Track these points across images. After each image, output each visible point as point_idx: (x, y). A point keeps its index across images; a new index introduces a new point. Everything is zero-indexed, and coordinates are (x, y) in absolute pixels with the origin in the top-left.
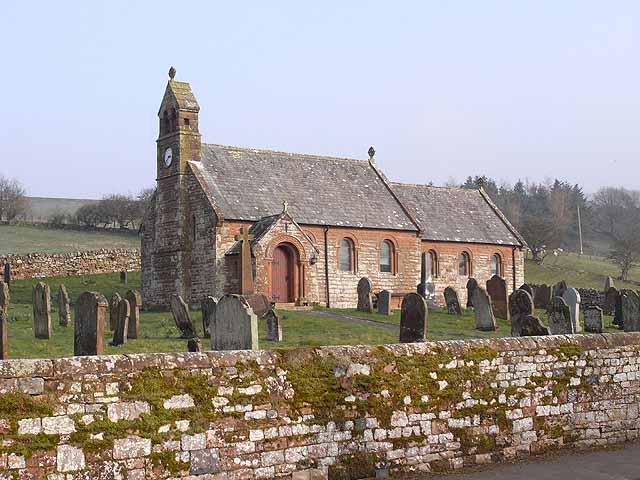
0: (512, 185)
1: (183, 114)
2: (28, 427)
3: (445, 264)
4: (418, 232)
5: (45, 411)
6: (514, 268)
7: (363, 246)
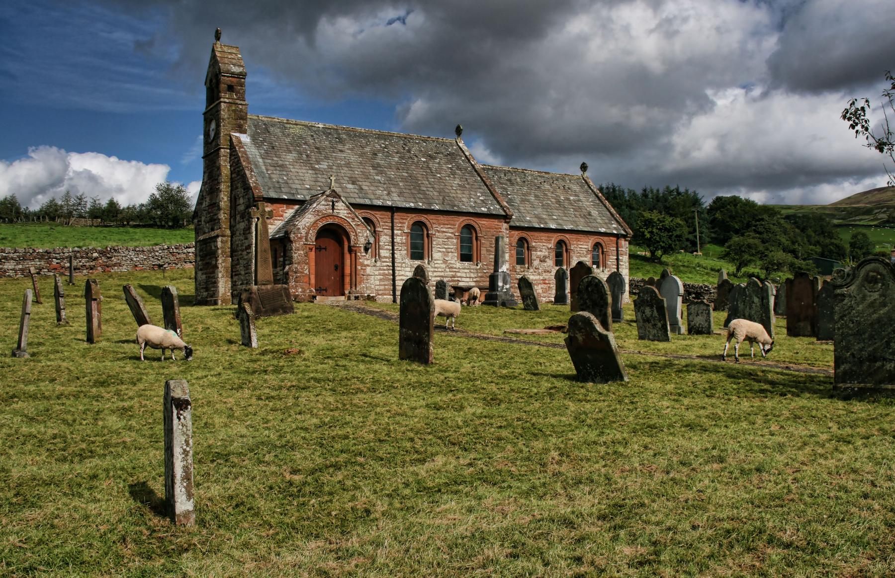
0: (639, 192)
1: (225, 80)
2: (838, 291)
3: (539, 253)
4: (506, 218)
5: (61, 410)
6: (617, 259)
7: (439, 232)
